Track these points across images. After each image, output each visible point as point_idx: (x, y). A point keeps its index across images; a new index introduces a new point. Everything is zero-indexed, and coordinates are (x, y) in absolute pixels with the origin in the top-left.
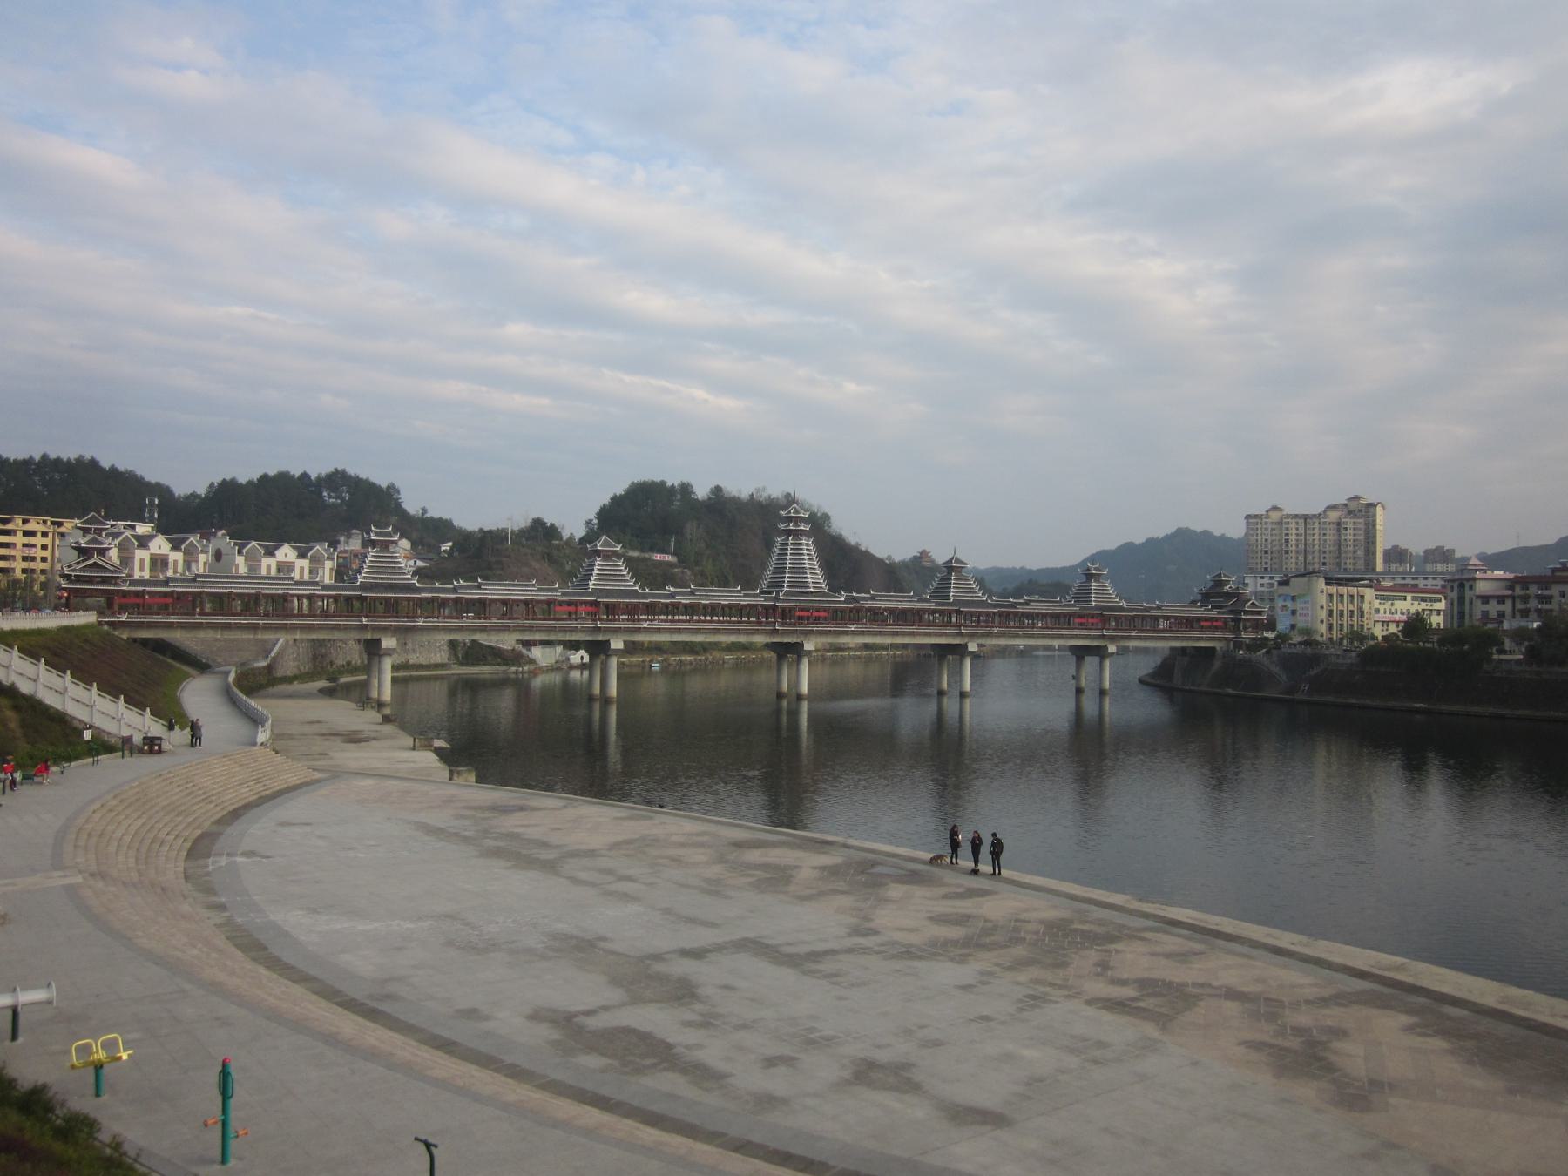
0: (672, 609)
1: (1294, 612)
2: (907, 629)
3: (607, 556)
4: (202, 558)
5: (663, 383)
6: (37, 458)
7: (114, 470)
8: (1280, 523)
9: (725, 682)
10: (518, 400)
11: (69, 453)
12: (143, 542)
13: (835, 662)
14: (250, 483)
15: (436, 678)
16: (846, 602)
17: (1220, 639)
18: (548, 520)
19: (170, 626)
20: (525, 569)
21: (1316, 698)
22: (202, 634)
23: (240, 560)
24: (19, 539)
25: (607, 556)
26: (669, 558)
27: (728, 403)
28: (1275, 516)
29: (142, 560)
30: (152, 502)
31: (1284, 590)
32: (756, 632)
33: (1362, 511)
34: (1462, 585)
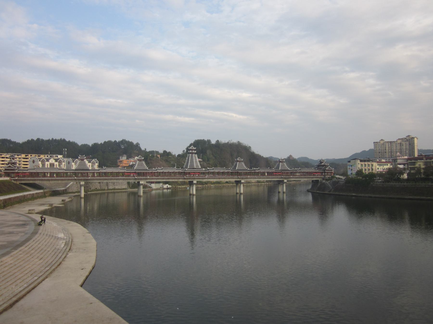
0: (209, 173)
1: (352, 170)
3: (240, 161)
4: (63, 163)
5: (225, 113)
6: (51, 139)
7: (69, 141)
8: (383, 144)
9: (212, 192)
10: (187, 119)
11: (58, 138)
12: (48, 160)
14: (101, 144)
15: (124, 192)
16: (205, 170)
17: (319, 178)
19: (35, 180)
21: (337, 193)
22: (51, 182)
23: (73, 164)
24: (18, 159)
25: (240, 161)
27: (241, 117)
28: (382, 142)
29: (47, 165)
30: (65, 150)
31: (349, 164)
32: (179, 179)
33: (410, 141)
34: (395, 161)
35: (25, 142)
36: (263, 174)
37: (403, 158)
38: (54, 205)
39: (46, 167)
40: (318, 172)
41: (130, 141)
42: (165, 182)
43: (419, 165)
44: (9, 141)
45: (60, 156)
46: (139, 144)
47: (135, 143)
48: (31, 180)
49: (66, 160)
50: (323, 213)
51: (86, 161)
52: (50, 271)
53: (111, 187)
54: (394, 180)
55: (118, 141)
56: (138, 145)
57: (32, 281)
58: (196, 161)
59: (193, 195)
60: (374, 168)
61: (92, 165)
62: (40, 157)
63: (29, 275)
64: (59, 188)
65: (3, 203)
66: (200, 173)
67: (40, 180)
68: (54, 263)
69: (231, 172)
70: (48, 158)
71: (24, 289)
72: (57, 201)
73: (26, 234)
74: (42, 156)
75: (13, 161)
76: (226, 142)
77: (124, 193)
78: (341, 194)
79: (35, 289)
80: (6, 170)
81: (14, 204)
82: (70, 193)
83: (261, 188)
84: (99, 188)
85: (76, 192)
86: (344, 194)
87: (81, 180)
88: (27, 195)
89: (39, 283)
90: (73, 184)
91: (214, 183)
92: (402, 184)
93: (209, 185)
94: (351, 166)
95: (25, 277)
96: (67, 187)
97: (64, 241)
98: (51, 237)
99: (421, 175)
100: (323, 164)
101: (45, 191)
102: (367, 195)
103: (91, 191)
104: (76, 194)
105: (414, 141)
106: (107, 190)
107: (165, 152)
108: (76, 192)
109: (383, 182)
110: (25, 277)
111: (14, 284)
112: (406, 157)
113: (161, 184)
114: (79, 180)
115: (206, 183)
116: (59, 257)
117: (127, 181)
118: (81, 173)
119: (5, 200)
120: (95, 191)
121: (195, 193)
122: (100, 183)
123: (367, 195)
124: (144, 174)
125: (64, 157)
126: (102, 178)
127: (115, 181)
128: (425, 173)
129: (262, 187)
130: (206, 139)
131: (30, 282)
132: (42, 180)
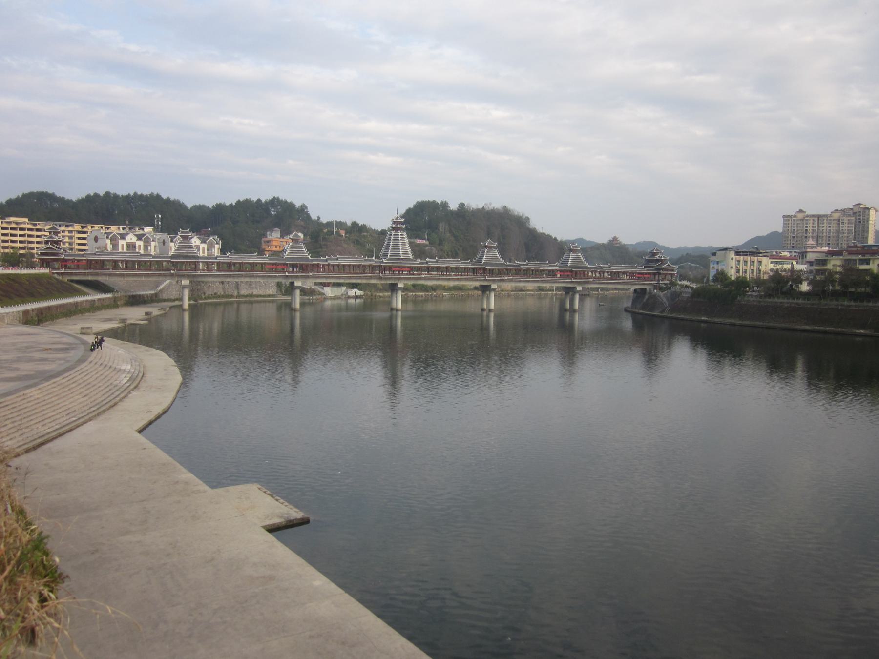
2: (91, 271)
3: (490, 248)
4: (153, 244)
6: (132, 194)
7: (168, 199)
8: (803, 220)
12: (123, 237)
13: (517, 298)
14: (231, 205)
15: (269, 301)
16: (421, 263)
17: (647, 284)
18: (361, 223)
19: (97, 275)
20: (339, 248)
21: (674, 315)
23: (172, 244)
24: (67, 233)
25: (490, 248)
26: (424, 242)
28: (800, 216)
29: (123, 245)
31: (713, 258)
32: (371, 278)
35: (83, 200)
36: (552, 274)
37: (819, 249)
38: (129, 322)
39: (120, 250)
40: (646, 274)
41: (289, 201)
42: (352, 284)
43: (834, 265)
44: (51, 197)
45: (148, 230)
46: (306, 208)
47: (298, 204)
48: (88, 274)
49: (159, 236)
50: (652, 356)
51: (195, 241)
52: (96, 413)
53: (244, 292)
54: (783, 293)
55: (263, 201)
56: (303, 208)
57: (68, 422)
58: (403, 246)
59: (397, 310)
60: (763, 268)
61: (204, 247)
62: (109, 231)
63: (64, 414)
64: (144, 290)
65: (37, 315)
66: (411, 269)
67: (105, 275)
68: (104, 402)
69: (473, 269)
70: (124, 232)
71: (54, 431)
72: (135, 315)
73: (68, 361)
74: (114, 230)
75: (56, 238)
76: (480, 207)
77: (271, 304)
78: (682, 316)
79: (72, 432)
80: (42, 254)
81: (57, 318)
82: (164, 300)
83: (546, 303)
84: (220, 292)
85: (177, 299)
86: (687, 317)
87: (183, 276)
88: (82, 302)
89: (78, 426)
90: (171, 284)
91: (450, 289)
92: (796, 301)
93: (439, 292)
94: (718, 263)
95: (58, 417)
96: (159, 289)
97: (129, 375)
98: (107, 368)
99: (833, 286)
100: (656, 257)
101: (116, 295)
102: (728, 321)
103: (205, 299)
104: (177, 303)
105: (869, 215)
106: (237, 297)
107: (355, 224)
108: (177, 299)
109: (761, 297)
110: (58, 417)
111: (41, 424)
112: (826, 249)
113: (344, 288)
114: (179, 276)
115: (433, 289)
116: (114, 396)
117: (277, 280)
118: (184, 264)
119: (40, 311)
120: (214, 298)
121: (400, 306)
122: (222, 283)
123: (728, 321)
124: (303, 268)
125: (156, 231)
126: (223, 273)
127: (253, 280)
128: (841, 282)
129: (548, 301)
130: (439, 201)
131: (65, 423)
132: (110, 275)
